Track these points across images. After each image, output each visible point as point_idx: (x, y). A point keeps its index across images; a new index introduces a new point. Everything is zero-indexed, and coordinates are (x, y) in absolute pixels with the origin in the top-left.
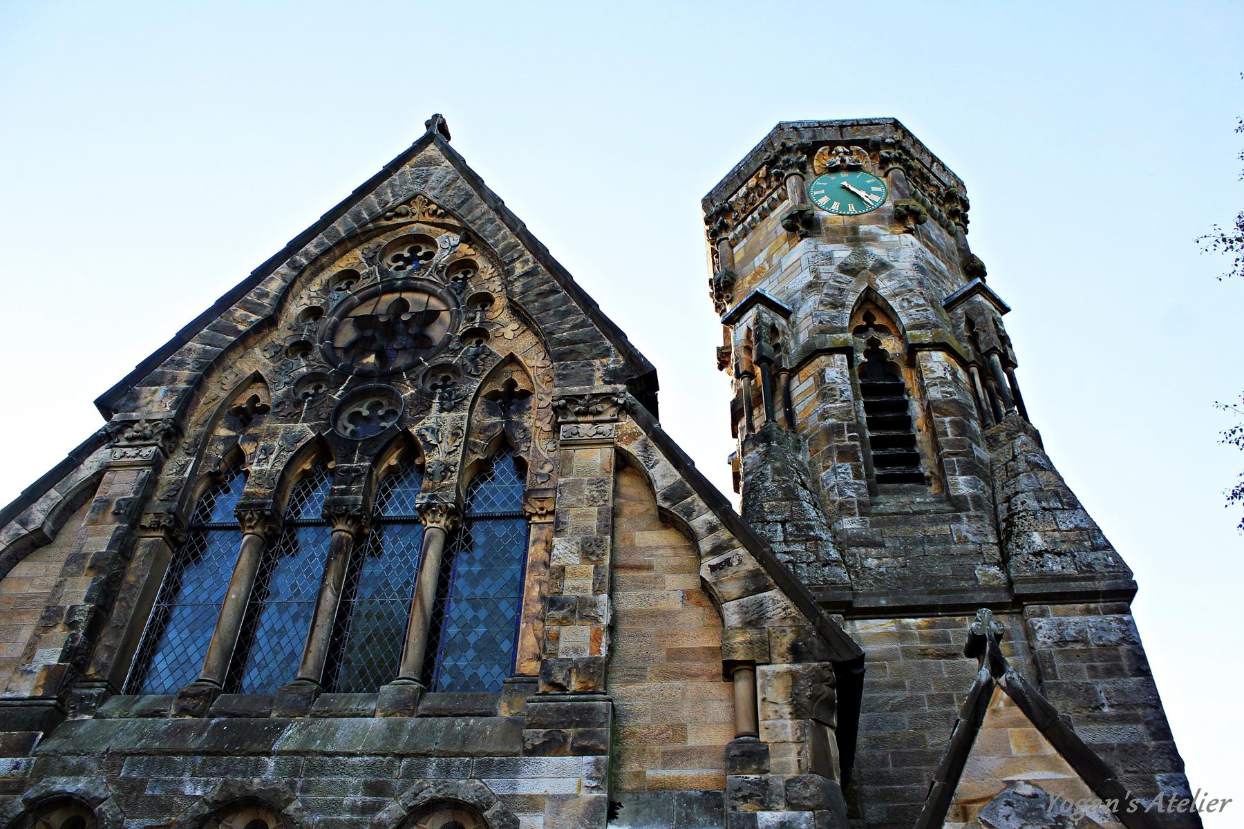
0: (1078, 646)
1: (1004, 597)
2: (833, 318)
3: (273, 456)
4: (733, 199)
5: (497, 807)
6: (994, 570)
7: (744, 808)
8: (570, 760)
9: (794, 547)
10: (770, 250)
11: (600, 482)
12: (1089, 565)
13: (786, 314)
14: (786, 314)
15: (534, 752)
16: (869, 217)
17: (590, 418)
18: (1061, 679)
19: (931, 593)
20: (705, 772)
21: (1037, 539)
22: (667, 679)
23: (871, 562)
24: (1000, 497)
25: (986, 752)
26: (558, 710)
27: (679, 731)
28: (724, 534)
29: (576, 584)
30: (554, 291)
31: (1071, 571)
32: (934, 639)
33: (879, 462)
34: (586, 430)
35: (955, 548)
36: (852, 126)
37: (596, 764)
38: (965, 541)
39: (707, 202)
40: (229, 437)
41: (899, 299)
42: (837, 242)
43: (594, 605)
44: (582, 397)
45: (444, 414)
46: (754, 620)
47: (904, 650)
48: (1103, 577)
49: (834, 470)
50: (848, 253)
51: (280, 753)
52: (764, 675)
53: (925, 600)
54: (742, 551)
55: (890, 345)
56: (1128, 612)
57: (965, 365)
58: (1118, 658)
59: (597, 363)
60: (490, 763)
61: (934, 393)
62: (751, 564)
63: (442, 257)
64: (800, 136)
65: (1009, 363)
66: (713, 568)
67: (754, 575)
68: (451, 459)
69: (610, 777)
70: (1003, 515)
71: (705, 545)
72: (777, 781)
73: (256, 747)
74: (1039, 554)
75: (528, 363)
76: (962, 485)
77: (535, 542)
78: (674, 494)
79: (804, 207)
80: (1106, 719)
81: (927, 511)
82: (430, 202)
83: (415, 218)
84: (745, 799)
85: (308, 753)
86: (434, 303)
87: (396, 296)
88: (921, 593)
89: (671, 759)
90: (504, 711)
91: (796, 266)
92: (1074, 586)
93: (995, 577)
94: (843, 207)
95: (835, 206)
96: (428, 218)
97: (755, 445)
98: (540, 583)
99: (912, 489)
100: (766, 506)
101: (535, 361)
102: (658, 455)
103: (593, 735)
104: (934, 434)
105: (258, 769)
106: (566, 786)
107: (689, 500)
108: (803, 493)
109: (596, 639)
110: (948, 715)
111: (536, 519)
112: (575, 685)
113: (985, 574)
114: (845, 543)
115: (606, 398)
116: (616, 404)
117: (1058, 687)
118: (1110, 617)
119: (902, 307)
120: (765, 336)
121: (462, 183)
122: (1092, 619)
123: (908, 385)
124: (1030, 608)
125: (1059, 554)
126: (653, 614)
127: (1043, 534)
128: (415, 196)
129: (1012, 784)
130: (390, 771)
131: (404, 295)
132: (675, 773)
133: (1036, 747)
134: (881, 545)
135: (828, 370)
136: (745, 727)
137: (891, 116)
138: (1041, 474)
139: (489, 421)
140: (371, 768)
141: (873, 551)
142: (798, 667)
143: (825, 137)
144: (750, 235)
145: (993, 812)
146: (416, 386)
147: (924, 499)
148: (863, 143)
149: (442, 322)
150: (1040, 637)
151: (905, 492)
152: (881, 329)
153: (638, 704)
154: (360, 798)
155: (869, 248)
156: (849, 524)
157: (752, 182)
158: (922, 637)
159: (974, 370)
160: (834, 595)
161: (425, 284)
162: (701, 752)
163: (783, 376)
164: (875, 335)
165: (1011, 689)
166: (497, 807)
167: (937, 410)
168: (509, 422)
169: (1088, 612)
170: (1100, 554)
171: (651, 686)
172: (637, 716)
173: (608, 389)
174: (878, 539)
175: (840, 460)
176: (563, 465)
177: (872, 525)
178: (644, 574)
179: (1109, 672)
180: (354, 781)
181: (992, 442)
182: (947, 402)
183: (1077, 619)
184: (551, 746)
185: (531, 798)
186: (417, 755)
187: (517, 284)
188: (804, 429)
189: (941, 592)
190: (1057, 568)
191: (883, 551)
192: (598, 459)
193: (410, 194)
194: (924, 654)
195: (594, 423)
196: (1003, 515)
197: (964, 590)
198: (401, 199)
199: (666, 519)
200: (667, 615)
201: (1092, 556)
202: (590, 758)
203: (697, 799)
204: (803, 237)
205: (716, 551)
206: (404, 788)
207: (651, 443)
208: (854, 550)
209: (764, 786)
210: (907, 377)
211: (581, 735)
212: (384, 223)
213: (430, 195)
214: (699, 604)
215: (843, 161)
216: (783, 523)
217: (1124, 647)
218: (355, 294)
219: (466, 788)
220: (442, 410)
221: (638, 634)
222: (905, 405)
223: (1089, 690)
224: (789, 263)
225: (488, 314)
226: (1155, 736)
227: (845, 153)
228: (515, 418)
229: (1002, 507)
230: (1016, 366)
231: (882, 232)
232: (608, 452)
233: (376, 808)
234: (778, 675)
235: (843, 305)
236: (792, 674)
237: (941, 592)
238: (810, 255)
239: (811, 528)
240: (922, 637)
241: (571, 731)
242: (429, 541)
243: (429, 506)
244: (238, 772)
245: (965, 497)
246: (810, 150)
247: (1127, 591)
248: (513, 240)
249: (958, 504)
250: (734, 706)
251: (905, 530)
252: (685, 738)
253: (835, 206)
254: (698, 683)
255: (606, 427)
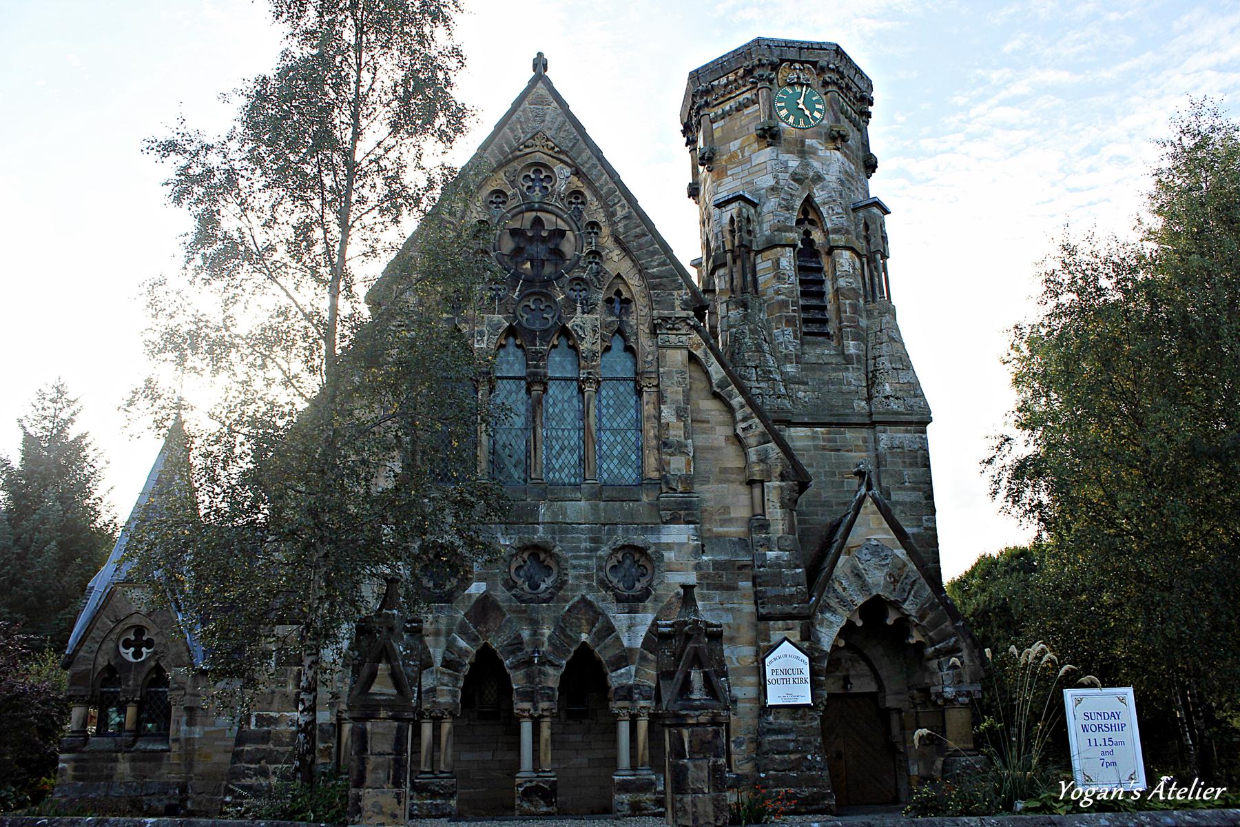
0: (899, 450)
1: (867, 421)
2: (787, 219)
3: (486, 338)
4: (716, 83)
5: (653, 549)
6: (863, 403)
7: (761, 550)
8: (683, 526)
9: (762, 385)
10: (743, 141)
11: (681, 373)
12: (911, 406)
13: (755, 205)
14: (755, 205)
15: (666, 523)
16: (813, 132)
17: (675, 332)
18: (889, 467)
19: (831, 415)
20: (739, 529)
21: (887, 387)
22: (721, 483)
23: (801, 394)
24: (870, 355)
25: (860, 526)
26: (676, 502)
27: (726, 509)
28: (748, 410)
29: (675, 433)
30: (644, 235)
31: (902, 409)
32: (829, 440)
33: (806, 321)
34: (673, 338)
35: (845, 388)
36: (808, 48)
37: (696, 529)
38: (849, 384)
39: (695, 76)
40: (449, 318)
41: (827, 207)
42: (791, 153)
43: (686, 446)
44: (670, 318)
45: (585, 315)
46: (763, 459)
47: (814, 446)
48: (917, 414)
49: (783, 331)
50: (797, 163)
51: (544, 523)
52: (768, 487)
53: (827, 420)
54: (757, 420)
55: (817, 236)
56: (925, 432)
57: (859, 256)
58: (917, 457)
59: (675, 293)
60: (647, 528)
61: (842, 283)
62: (761, 428)
63: (561, 187)
64: (772, 53)
65: (885, 256)
66: (744, 429)
67: (763, 434)
68: (594, 347)
69: (699, 534)
70: (871, 368)
71: (739, 416)
72: (774, 537)
73: (531, 520)
74: (887, 397)
75: (630, 282)
76: (852, 347)
77: (647, 403)
78: (722, 384)
79: (772, 123)
80: (906, 489)
81: (831, 363)
82: (548, 140)
83: (537, 149)
84: (761, 546)
85: (557, 523)
86: (562, 225)
87: (534, 214)
88: (826, 415)
89: (724, 522)
90: (645, 499)
91: (762, 167)
92: (903, 418)
93: (863, 408)
94: (796, 121)
95: (791, 119)
96: (546, 150)
97: (737, 308)
98: (653, 428)
99: (824, 343)
100: (746, 355)
101: (634, 282)
102: (713, 359)
103: (693, 515)
104: (839, 310)
105: (535, 531)
106: (683, 538)
107: (730, 388)
108: (766, 347)
109: (688, 464)
110: (833, 482)
111: (645, 389)
112: (680, 489)
113: (858, 406)
114: (788, 380)
115: (684, 319)
116: (689, 324)
117: (886, 471)
118: (917, 435)
119: (828, 213)
120: (741, 226)
121: (568, 126)
122: (908, 435)
123: (826, 269)
124: (879, 428)
125: (897, 398)
126: (712, 448)
127: (891, 384)
128: (537, 134)
129: (869, 540)
130: (600, 532)
131: (539, 214)
132: (725, 529)
133: (881, 523)
134: (807, 384)
135: (782, 259)
136: (759, 511)
137: (835, 42)
138: (894, 344)
139: (609, 319)
140: (591, 530)
141: (802, 387)
142: (783, 484)
143: (789, 56)
144: (727, 119)
145: (860, 552)
146: (564, 293)
147: (827, 351)
148: (814, 64)
149: (568, 240)
150: (881, 444)
151: (818, 344)
152: (812, 222)
153: (707, 495)
154: (588, 545)
155: (811, 160)
156: (790, 368)
157: (732, 77)
158: (824, 439)
159: (865, 260)
160: (783, 416)
161: (555, 209)
162: (737, 519)
163: (752, 254)
164: (809, 227)
165: (873, 497)
166: (653, 549)
167: (843, 295)
168: (621, 321)
169: (907, 432)
170: (917, 400)
171: (712, 487)
172: (707, 502)
173: (683, 314)
174: (805, 380)
175: (786, 326)
176: (659, 361)
177: (802, 370)
178: (705, 425)
179: (911, 465)
180: (584, 537)
181: (869, 314)
182: (848, 290)
183: (900, 435)
184: (674, 520)
185: (668, 544)
186: (612, 524)
187: (620, 225)
188: (763, 295)
189: (836, 415)
190: (896, 407)
191: (807, 387)
192: (677, 357)
193: (535, 131)
194: (824, 448)
195: (677, 335)
196: (871, 368)
197: (847, 415)
198: (529, 136)
199: (716, 396)
200: (719, 449)
201: (914, 400)
202: (692, 526)
203: (737, 543)
204: (768, 146)
205: (744, 419)
206: (609, 540)
207: (709, 351)
208: (792, 386)
209: (768, 539)
210: (825, 262)
211: (688, 515)
212: (518, 153)
213: (548, 134)
214: (733, 444)
215: (799, 78)
216: (756, 368)
217: (921, 452)
218: (508, 212)
219: (638, 540)
220: (583, 313)
221: (705, 459)
222: (822, 282)
223: (901, 474)
224: (758, 162)
225: (600, 240)
226: (926, 498)
227: (800, 69)
228: (624, 318)
229: (870, 375)
230: (871, 104)
231: (820, 147)
232: (686, 352)
233: (597, 549)
234: (775, 488)
235: (793, 208)
236: (781, 487)
237: (836, 415)
238: (774, 162)
239: (770, 372)
240: (824, 439)
241: (682, 512)
242: (589, 399)
243: (588, 379)
244: (525, 533)
245: (852, 355)
246: (775, 67)
247: (922, 420)
248: (612, 185)
249: (848, 360)
250: (752, 498)
251: (818, 374)
252: (729, 513)
253: (791, 119)
254: (734, 486)
255: (684, 338)
